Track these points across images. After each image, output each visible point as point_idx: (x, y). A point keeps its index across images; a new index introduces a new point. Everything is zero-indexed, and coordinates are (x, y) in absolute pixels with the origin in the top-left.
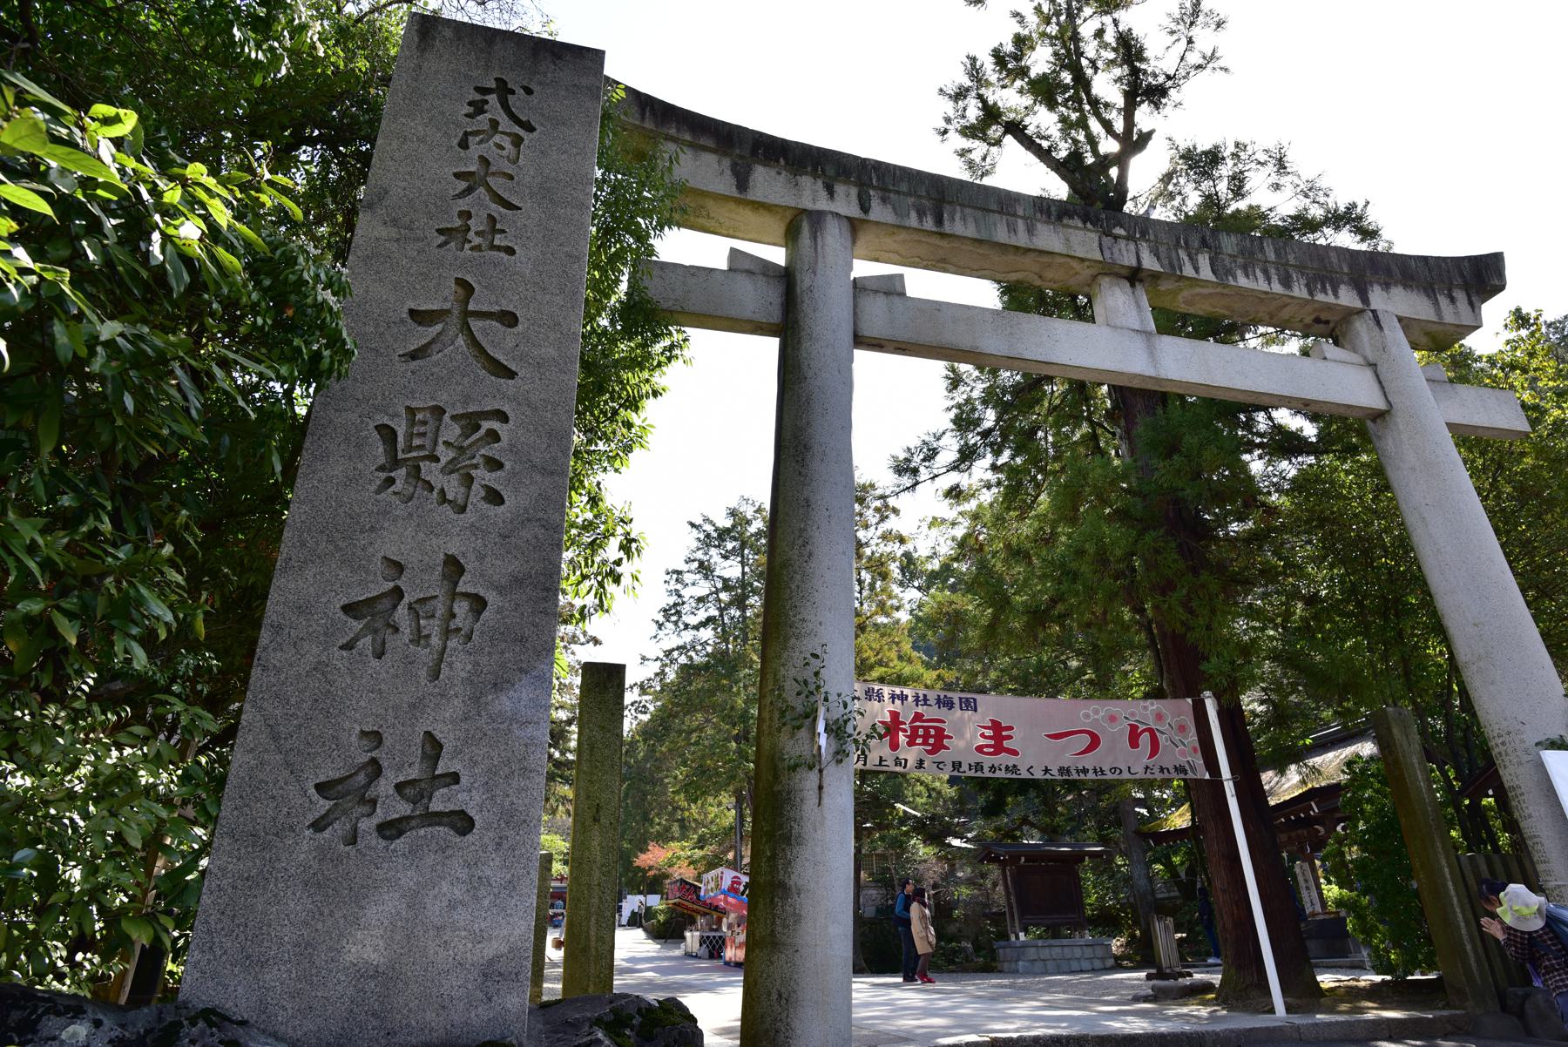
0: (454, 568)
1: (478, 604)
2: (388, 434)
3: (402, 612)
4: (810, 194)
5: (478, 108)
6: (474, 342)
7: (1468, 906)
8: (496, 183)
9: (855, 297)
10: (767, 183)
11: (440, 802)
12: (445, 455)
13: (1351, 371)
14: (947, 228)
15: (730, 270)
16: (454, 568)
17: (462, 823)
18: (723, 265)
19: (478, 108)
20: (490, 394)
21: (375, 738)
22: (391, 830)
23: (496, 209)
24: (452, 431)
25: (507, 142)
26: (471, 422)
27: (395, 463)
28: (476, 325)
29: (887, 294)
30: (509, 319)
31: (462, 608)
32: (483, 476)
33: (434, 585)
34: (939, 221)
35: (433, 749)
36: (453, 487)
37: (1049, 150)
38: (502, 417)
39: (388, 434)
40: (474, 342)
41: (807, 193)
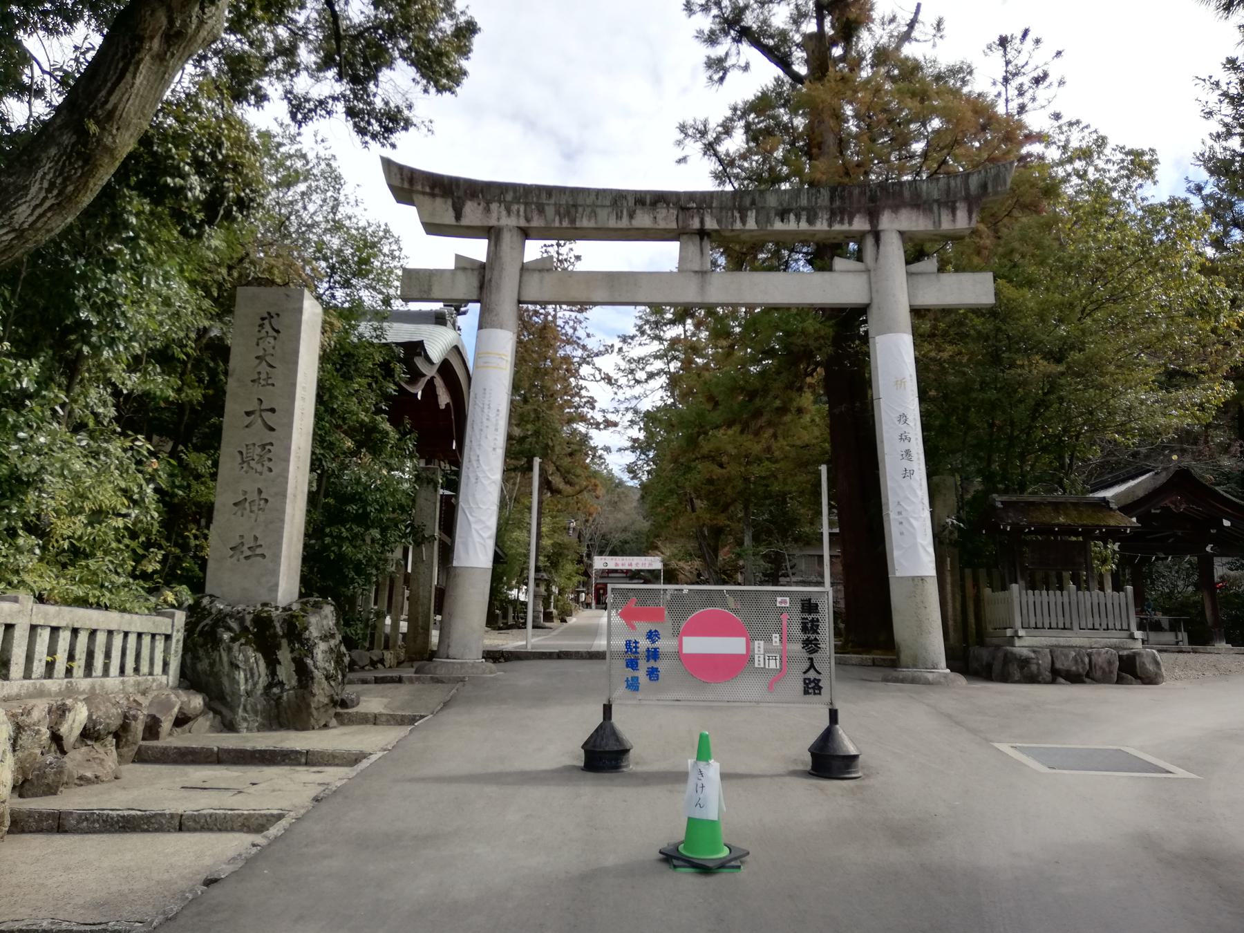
0: (260, 491)
1: (266, 501)
2: (241, 453)
3: (247, 505)
4: (499, 217)
5: (261, 326)
6: (263, 420)
7: (958, 597)
8: (268, 358)
9: (521, 276)
10: (473, 213)
11: (259, 551)
12: (256, 458)
13: (850, 277)
14: (578, 224)
15: (457, 268)
16: (260, 491)
17: (263, 556)
18: (451, 265)
19: (261, 326)
20: (268, 437)
21: (242, 537)
22: (247, 558)
23: (269, 369)
24: (258, 450)
25: (272, 340)
26: (263, 447)
27: (243, 462)
28: (264, 414)
29: (540, 271)
30: (273, 410)
31: (262, 502)
32: (267, 463)
33: (255, 496)
34: (573, 221)
35: (256, 538)
36: (259, 468)
37: (777, 47)
38: (271, 444)
39: (241, 453)
40: (263, 420)
41: (494, 215)
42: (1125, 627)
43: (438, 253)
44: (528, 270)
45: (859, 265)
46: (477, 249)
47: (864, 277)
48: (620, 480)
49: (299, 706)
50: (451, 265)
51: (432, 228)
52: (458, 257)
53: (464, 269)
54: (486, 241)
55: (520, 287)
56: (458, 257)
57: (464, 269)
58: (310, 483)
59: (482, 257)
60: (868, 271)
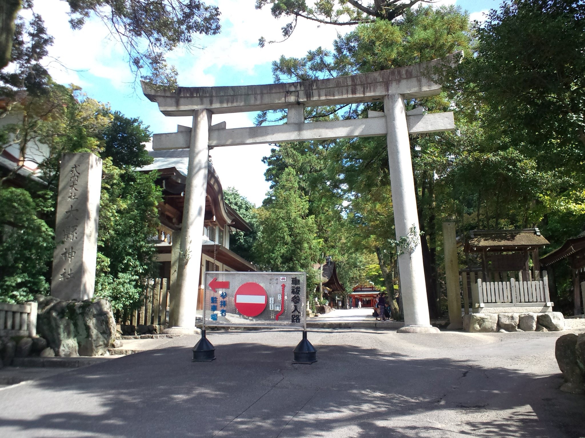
18: (175, 130)
42: (543, 300)
43: (169, 125)
44: (212, 130)
45: (381, 113)
46: (187, 121)
47: (384, 120)
48: (20, 27)
49: (391, 253)
50: (175, 130)
51: (167, 113)
52: (179, 126)
53: (182, 132)
54: (192, 117)
55: (350, 327)
56: (179, 126)
57: (182, 132)
58: (261, 270)
59: (190, 125)
60: (385, 116)
